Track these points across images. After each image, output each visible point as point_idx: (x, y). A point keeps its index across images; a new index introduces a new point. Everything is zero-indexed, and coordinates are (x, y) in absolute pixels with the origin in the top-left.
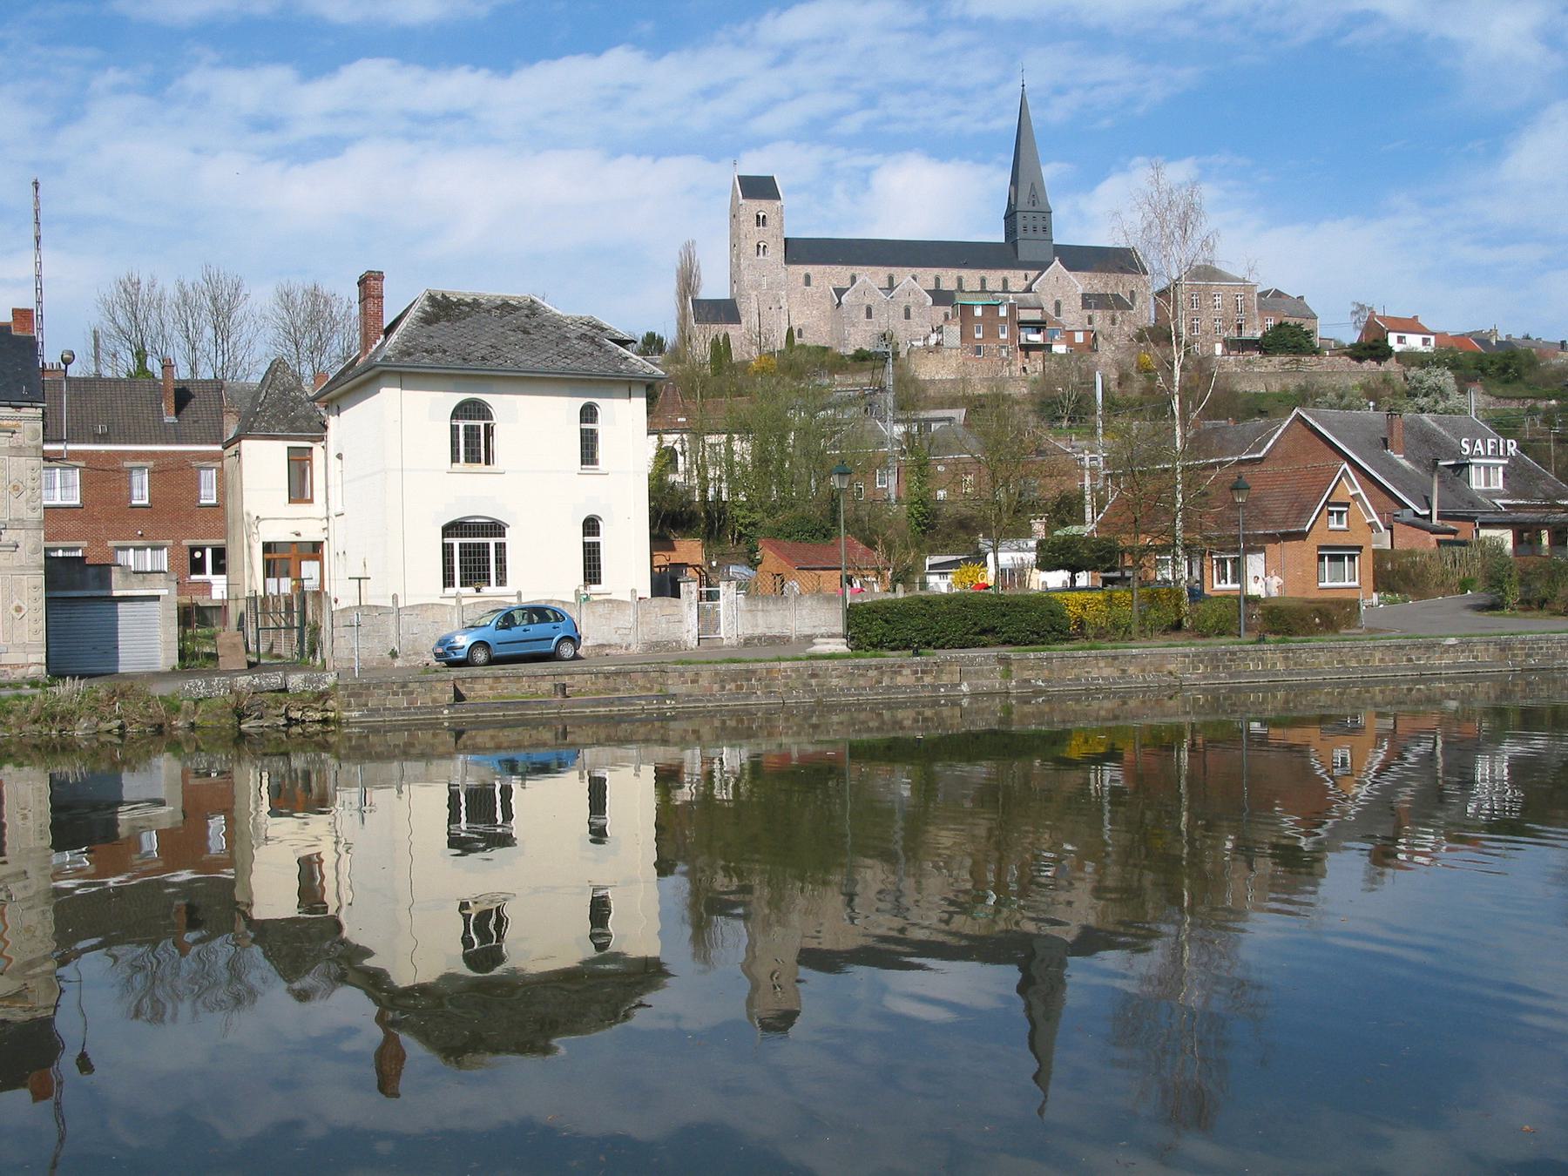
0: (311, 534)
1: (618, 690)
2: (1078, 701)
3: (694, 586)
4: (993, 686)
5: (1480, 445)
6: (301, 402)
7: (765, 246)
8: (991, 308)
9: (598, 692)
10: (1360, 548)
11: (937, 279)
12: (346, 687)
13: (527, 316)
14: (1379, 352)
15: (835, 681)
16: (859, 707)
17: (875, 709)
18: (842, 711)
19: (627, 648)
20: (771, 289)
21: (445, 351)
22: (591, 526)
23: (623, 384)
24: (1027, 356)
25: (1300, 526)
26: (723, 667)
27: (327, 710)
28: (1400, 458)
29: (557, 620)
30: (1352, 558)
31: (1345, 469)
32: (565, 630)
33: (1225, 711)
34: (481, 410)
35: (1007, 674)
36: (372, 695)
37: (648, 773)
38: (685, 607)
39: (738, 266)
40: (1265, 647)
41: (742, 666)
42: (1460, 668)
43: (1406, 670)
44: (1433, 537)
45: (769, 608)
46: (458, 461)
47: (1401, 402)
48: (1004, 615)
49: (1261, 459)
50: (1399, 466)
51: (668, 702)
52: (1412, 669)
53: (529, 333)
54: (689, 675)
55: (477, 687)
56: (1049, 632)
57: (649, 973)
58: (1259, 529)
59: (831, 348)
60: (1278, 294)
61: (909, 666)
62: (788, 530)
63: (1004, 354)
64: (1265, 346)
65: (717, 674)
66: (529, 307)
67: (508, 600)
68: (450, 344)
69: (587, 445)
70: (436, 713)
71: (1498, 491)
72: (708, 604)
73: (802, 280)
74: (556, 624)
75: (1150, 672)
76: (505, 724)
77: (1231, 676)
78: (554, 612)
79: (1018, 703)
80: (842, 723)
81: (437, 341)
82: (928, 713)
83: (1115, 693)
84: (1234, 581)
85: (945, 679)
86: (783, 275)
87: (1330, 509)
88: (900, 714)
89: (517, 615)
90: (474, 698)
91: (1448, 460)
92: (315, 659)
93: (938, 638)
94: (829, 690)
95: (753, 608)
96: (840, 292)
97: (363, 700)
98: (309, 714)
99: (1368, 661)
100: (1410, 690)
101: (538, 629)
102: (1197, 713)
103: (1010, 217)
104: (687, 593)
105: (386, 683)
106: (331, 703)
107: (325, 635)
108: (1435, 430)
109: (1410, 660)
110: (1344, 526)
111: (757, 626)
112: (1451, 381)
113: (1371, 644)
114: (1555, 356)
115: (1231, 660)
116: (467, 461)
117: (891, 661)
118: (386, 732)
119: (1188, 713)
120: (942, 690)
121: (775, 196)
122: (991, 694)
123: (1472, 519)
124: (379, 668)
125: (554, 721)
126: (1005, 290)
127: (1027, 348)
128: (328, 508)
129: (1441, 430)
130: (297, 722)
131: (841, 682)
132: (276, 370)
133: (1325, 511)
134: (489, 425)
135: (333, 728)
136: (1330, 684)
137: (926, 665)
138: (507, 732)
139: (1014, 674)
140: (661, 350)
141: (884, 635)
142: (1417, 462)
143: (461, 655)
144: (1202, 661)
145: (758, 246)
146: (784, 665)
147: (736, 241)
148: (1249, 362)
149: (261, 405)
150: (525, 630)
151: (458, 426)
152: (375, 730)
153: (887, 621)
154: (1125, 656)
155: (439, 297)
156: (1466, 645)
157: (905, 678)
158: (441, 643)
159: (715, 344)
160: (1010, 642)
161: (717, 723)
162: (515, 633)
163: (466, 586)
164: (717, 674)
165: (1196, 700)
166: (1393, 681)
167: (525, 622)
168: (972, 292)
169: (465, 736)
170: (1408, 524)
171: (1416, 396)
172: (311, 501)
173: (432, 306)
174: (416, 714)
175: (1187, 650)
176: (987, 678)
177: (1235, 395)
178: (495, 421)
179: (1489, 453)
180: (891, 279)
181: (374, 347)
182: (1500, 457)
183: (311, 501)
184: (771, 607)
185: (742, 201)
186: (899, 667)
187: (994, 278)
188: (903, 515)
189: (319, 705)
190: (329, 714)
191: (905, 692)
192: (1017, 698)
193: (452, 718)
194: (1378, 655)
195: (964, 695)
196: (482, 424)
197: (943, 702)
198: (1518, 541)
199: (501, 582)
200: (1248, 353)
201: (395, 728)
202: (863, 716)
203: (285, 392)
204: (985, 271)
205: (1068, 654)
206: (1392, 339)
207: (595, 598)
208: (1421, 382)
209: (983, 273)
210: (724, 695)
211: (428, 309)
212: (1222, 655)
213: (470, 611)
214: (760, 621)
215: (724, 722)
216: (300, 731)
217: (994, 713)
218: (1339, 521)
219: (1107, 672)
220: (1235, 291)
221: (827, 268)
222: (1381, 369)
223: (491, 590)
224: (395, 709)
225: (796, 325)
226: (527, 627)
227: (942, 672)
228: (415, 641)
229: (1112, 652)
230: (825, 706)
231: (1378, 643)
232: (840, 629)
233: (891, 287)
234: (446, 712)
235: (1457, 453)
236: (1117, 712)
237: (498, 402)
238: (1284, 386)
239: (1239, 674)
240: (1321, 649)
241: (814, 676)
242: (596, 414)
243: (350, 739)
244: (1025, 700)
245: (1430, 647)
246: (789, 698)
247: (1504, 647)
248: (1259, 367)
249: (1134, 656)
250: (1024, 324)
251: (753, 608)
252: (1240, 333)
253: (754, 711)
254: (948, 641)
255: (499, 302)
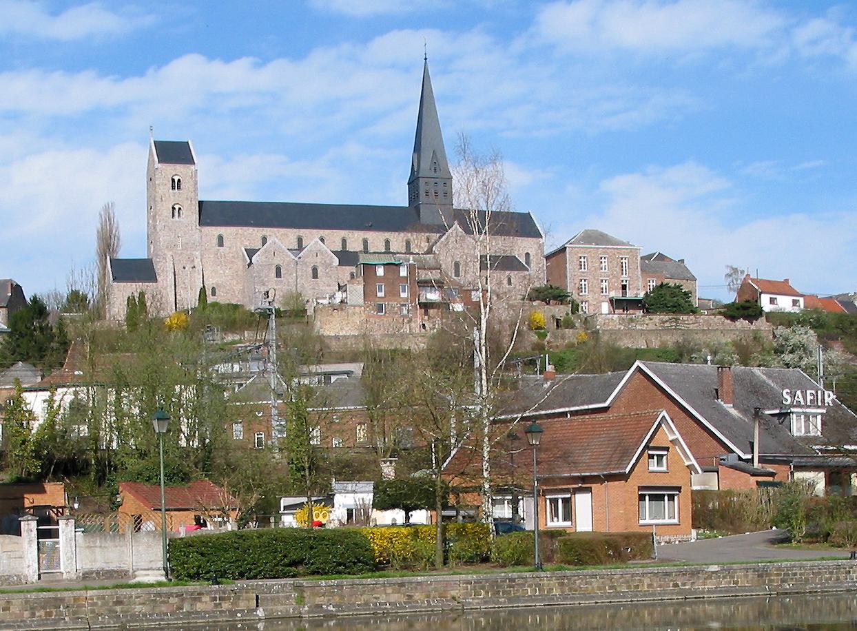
3: (34, 524)
4: (287, 611)
5: (800, 396)
7: (180, 209)
8: (392, 267)
10: (679, 489)
11: (344, 241)
14: (750, 312)
15: (138, 608)
24: (426, 313)
25: (622, 468)
26: (33, 596)
28: (729, 408)
30: (671, 498)
31: (664, 417)
35: (301, 600)
38: (26, 545)
39: (154, 228)
40: (542, 574)
41: (51, 595)
42: (720, 592)
43: (673, 594)
44: (753, 479)
45: (107, 545)
48: (312, 548)
49: (605, 410)
50: (727, 414)
52: (677, 594)
56: (355, 563)
59: (242, 306)
60: (661, 257)
61: (209, 593)
63: (405, 312)
64: (647, 305)
71: (816, 438)
73: (215, 241)
75: (434, 597)
77: (510, 600)
83: (401, 617)
84: (565, 519)
85: (242, 605)
86: (197, 236)
87: (650, 452)
91: (773, 409)
93: (250, 570)
96: (251, 253)
103: (413, 183)
104: (28, 531)
108: (764, 382)
109: (676, 585)
110: (664, 468)
111: (95, 561)
113: (641, 571)
115: (510, 587)
117: (190, 589)
120: (239, 615)
123: (787, 463)
126: (408, 251)
127: (426, 306)
129: (770, 382)
131: (145, 609)
133: (646, 455)
136: (602, 607)
140: (85, 307)
141: (199, 567)
142: (744, 411)
144: (483, 588)
145: (174, 208)
146: (90, 593)
147: (152, 204)
148: (632, 320)
153: (202, 554)
154: (411, 583)
156: (727, 572)
157: (205, 604)
159: (130, 300)
160: (318, 573)
164: (27, 602)
170: (731, 467)
171: (782, 353)
175: (469, 577)
177: (617, 351)
179: (809, 403)
180: (300, 240)
182: (819, 407)
184: (109, 543)
185: (157, 165)
186: (198, 594)
187: (397, 241)
188: (285, 461)
191: (204, 617)
192: (309, 622)
194: (647, 581)
195: (260, 619)
197: (239, 626)
198: (829, 482)
200: (631, 311)
204: (389, 233)
205: (357, 581)
208: (787, 340)
209: (387, 235)
210: (33, 621)
212: (502, 581)
214: (99, 557)
218: (659, 463)
219: (394, 597)
220: (621, 254)
221: (240, 230)
225: (209, 285)
227: (239, 599)
229: (399, 580)
232: (161, 564)
233: (300, 247)
235: (780, 404)
238: (664, 344)
239: (517, 599)
241: (119, 603)
245: (694, 574)
247: (762, 574)
248: (641, 325)
250: (425, 284)
252: (624, 293)
254: (260, 572)
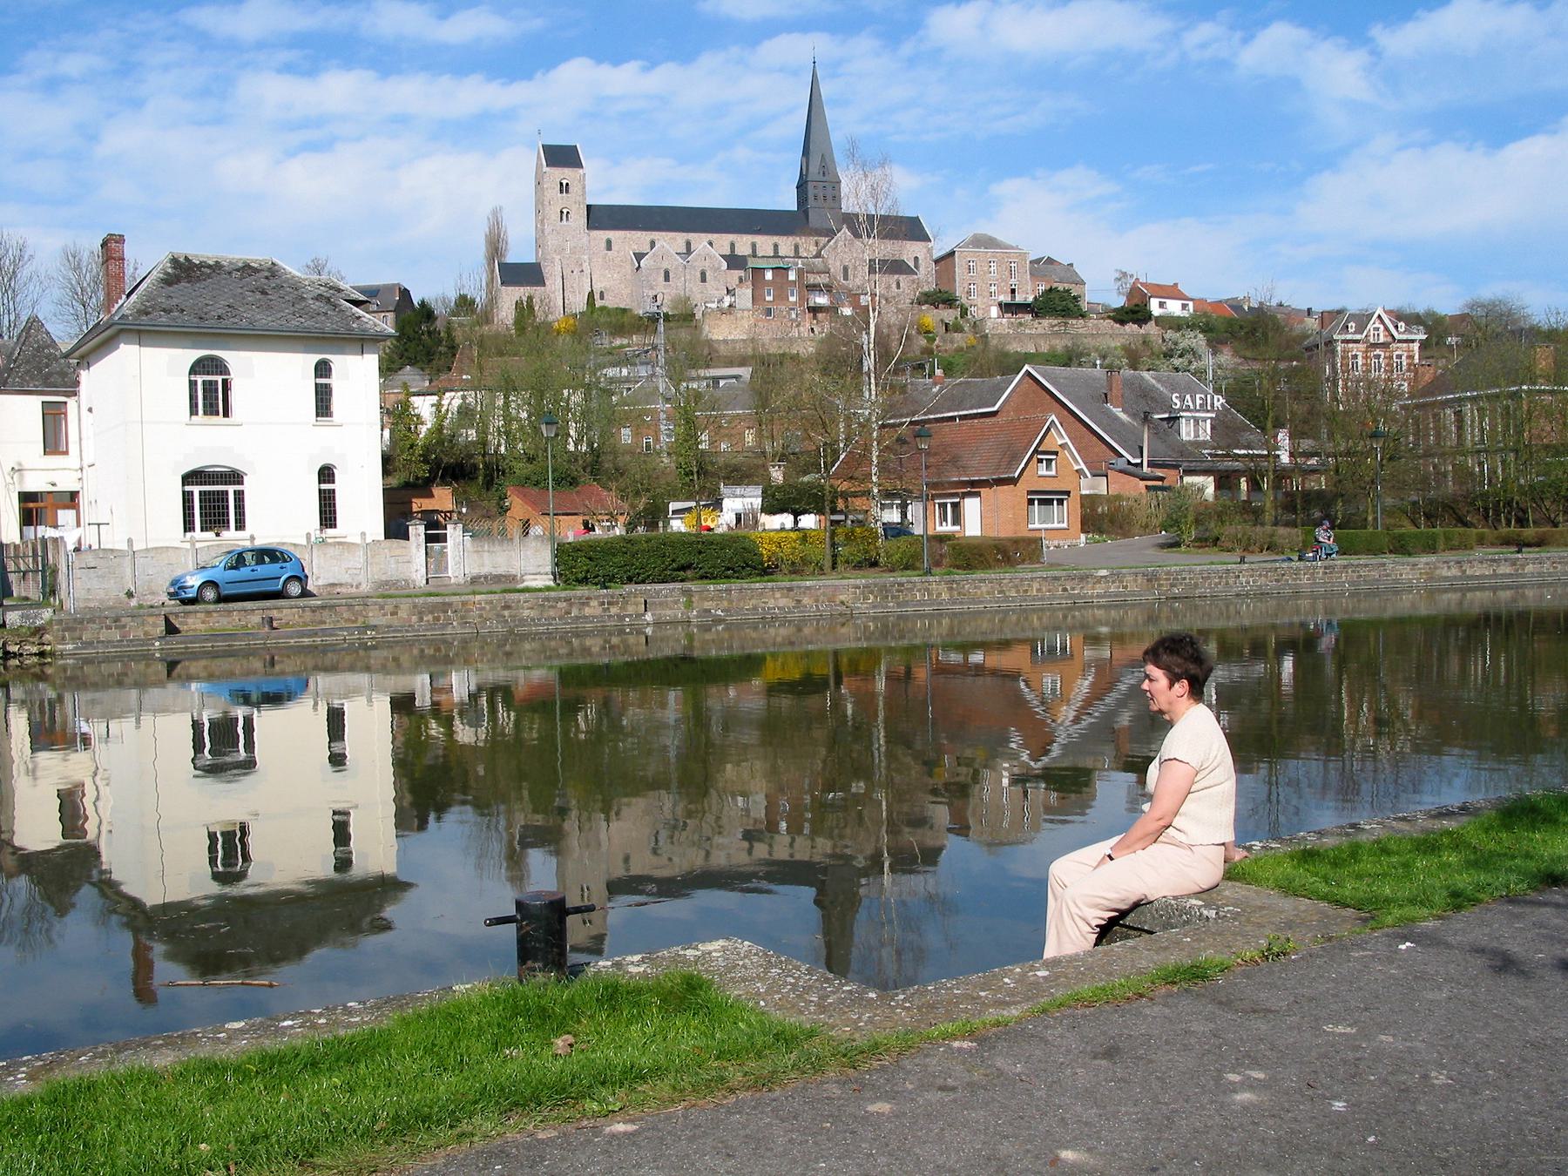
0: (66, 484)
1: (325, 623)
2: (755, 628)
3: (422, 529)
4: (676, 616)
6: (56, 358)
8: (781, 271)
9: (306, 624)
10: (1068, 493)
11: (733, 245)
12: (60, 622)
13: (267, 278)
14: (1139, 316)
15: (526, 613)
16: (550, 635)
17: (565, 638)
18: (533, 639)
19: (357, 587)
20: (574, 253)
21: (183, 311)
22: (326, 474)
23: (360, 342)
24: (815, 317)
25: (1011, 473)
26: (421, 600)
27: (44, 644)
28: (1118, 412)
29: (285, 561)
30: (1060, 502)
32: (292, 570)
33: (894, 638)
34: (217, 366)
35: (689, 605)
36: (86, 629)
37: (383, 705)
39: (543, 232)
40: (931, 579)
41: (439, 599)
42: (1110, 596)
44: (1143, 484)
46: (197, 414)
47: (1157, 362)
48: (700, 553)
50: (1117, 418)
51: (369, 632)
52: (1066, 598)
53: (267, 294)
54: (388, 608)
55: (190, 621)
56: (743, 568)
57: (389, 887)
58: (953, 476)
59: (631, 310)
60: (1050, 261)
61: (597, 598)
62: (535, 478)
63: (794, 316)
64: (1035, 309)
65: (415, 606)
66: (269, 270)
67: (241, 543)
68: (188, 304)
69: (322, 399)
70: (147, 645)
71: (1205, 442)
72: (437, 546)
73: (604, 245)
74: (284, 565)
76: (214, 655)
77: (899, 605)
78: (282, 553)
79: (698, 630)
80: (533, 651)
81: (175, 301)
82: (615, 640)
83: (790, 621)
85: (631, 609)
86: (585, 239)
87: (1039, 457)
88: (588, 642)
89: (248, 556)
90: (187, 631)
92: (55, 599)
93: (639, 574)
94: (521, 620)
95: (480, 549)
96: (639, 256)
97: (77, 634)
98: (26, 647)
99: (1026, 591)
100: (1065, 617)
101: (268, 569)
102: (868, 639)
103: (802, 187)
105: (99, 618)
106: (47, 637)
107: (62, 577)
109: (1065, 590)
110: (1053, 473)
112: (1203, 343)
114: (1302, 321)
115: (898, 591)
116: (205, 413)
117: (579, 593)
118: (99, 663)
119: (860, 639)
120: (627, 619)
121: (579, 165)
122: (674, 623)
123: (1176, 467)
124: (115, 607)
125: (261, 651)
126: (797, 255)
127: (815, 310)
128: (81, 460)
129: (1159, 386)
130: (15, 655)
131: (532, 613)
132: (30, 328)
133: (1035, 459)
134: (227, 380)
135: (50, 660)
137: (612, 597)
138: (219, 662)
139: (695, 605)
140: (473, 311)
141: (588, 571)
142: (1133, 416)
143: (191, 594)
144: (872, 592)
145: (562, 212)
146: (478, 597)
149: (15, 361)
150: (253, 571)
151: (196, 381)
152: (88, 661)
153: (590, 559)
154: (800, 588)
155: (182, 260)
156: (1116, 576)
157: (593, 609)
158: (173, 584)
159: (518, 304)
160: (706, 578)
161: (416, 652)
162: (244, 572)
163: (207, 531)
164: (415, 606)
165: (866, 627)
166: (1049, 609)
167: (253, 563)
168: (763, 257)
169: (179, 666)
171: (1171, 357)
172: (66, 453)
173: (174, 268)
174: (129, 646)
176: (671, 609)
177: (1006, 355)
178: (232, 376)
180: (688, 244)
181: (117, 306)
182: (1208, 411)
183: (66, 453)
184: (497, 548)
185: (545, 169)
187: (786, 244)
189: (36, 639)
190: (45, 647)
191: (592, 622)
192: (697, 626)
193: (162, 649)
194: (1036, 585)
195: (648, 624)
196: (219, 379)
197: (628, 630)
198: (1218, 487)
199: (240, 525)
200: (1020, 315)
201: (109, 659)
202: (553, 643)
203: (39, 349)
205: (745, 586)
206: (1154, 305)
207: (329, 540)
208: (1176, 344)
209: (776, 239)
211: (170, 270)
213: (203, 553)
214: (487, 562)
215: (422, 651)
216: (18, 663)
217: (678, 640)
218: (1048, 467)
219: (783, 602)
222: (1142, 331)
223: (231, 535)
224: (109, 642)
226: (255, 568)
228: (150, 581)
229: (788, 584)
230: (517, 635)
231: (1035, 575)
232: (549, 569)
233: (689, 251)
234: (157, 644)
235: (1170, 409)
236: (793, 639)
237: (235, 359)
239: (906, 604)
240: (984, 581)
241: (507, 607)
242: (330, 368)
243: (65, 670)
244: (705, 628)
245: (1083, 578)
246: (482, 628)
247: (1151, 579)
248: (1030, 329)
249: (808, 588)
250: (814, 288)
251: (480, 549)
252: (1013, 297)
253: (451, 641)
254: (649, 576)
255: (240, 265)
